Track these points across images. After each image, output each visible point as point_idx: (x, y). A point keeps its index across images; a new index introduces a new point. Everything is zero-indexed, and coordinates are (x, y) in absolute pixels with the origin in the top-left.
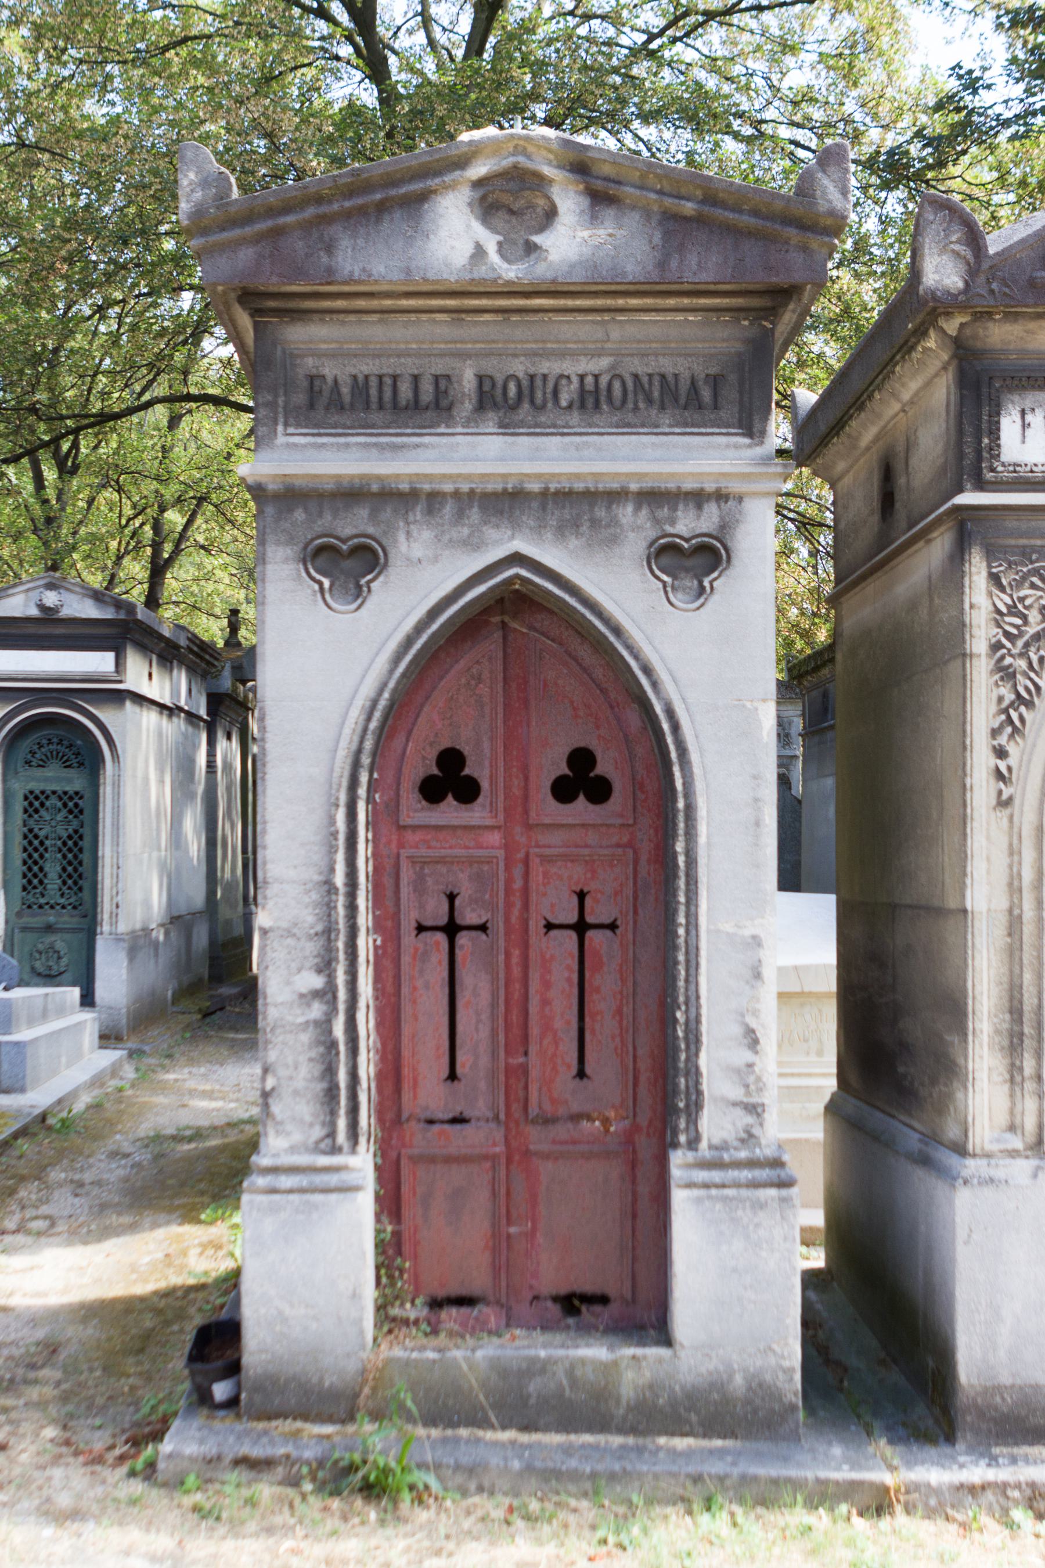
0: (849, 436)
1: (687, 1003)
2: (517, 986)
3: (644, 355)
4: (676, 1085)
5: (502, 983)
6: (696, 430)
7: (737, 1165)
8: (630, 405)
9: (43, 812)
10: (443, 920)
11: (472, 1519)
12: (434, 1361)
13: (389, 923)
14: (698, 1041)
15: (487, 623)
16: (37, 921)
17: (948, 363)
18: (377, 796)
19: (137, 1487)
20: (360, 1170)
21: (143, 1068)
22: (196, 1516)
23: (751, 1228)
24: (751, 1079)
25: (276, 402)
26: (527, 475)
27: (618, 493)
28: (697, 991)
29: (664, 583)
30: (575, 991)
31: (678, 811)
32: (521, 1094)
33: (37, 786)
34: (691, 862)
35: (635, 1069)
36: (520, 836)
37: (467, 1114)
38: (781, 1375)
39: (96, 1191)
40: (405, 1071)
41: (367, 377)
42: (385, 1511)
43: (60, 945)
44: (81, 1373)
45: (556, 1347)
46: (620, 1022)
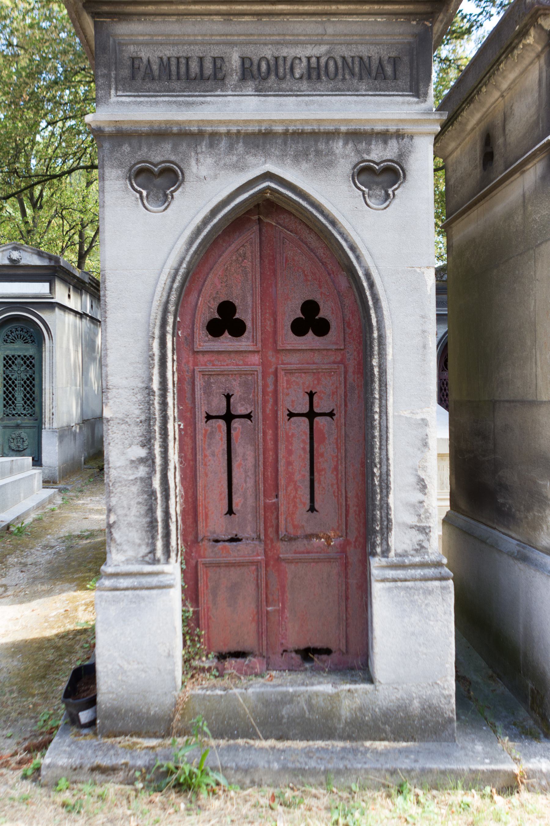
0: (460, 123)
1: (380, 463)
2: (271, 453)
3: (349, 44)
4: (374, 515)
5: (261, 451)
6: (382, 93)
7: (414, 566)
8: (340, 77)
9: (13, 366)
10: (223, 412)
11: (249, 804)
12: (221, 696)
13: (188, 415)
14: (388, 487)
15: (249, 220)
16: (12, 423)
17: (542, 52)
18: (180, 332)
19: (27, 787)
20: (171, 574)
21: (67, 498)
22: (64, 810)
23: (423, 606)
24: (422, 511)
25: (110, 74)
26: (274, 121)
27: (333, 133)
28: (387, 455)
29: (363, 192)
30: (308, 456)
31: (374, 339)
32: (274, 522)
33: (10, 353)
34: (383, 372)
35: (346, 505)
36: (271, 357)
38: (443, 700)
39: (33, 568)
40: (200, 509)
41: (169, 58)
42: (191, 802)
43: (23, 435)
44: (5, 695)
45: (299, 685)
46: (337, 475)
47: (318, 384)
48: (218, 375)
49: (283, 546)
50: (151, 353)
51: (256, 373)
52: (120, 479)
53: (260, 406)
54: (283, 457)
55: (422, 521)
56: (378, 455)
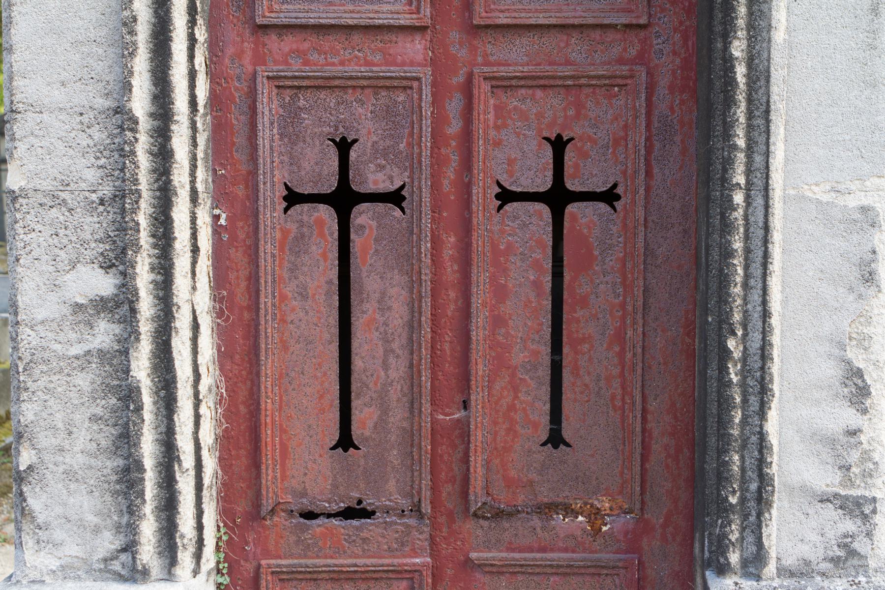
2: (452, 294)
10: (330, 185)
13: (240, 191)
14: (764, 390)
24: (854, 456)
28: (764, 303)
30: (547, 303)
32: (457, 469)
34: (760, 76)
35: (644, 430)
37: (369, 502)
40: (267, 434)
46: (621, 355)
47: (578, 116)
48: (318, 88)
49: (479, 532)
50: (126, 13)
51: (415, 84)
52: (46, 355)
53: (426, 172)
54: (484, 304)
55: (853, 485)
56: (739, 302)
